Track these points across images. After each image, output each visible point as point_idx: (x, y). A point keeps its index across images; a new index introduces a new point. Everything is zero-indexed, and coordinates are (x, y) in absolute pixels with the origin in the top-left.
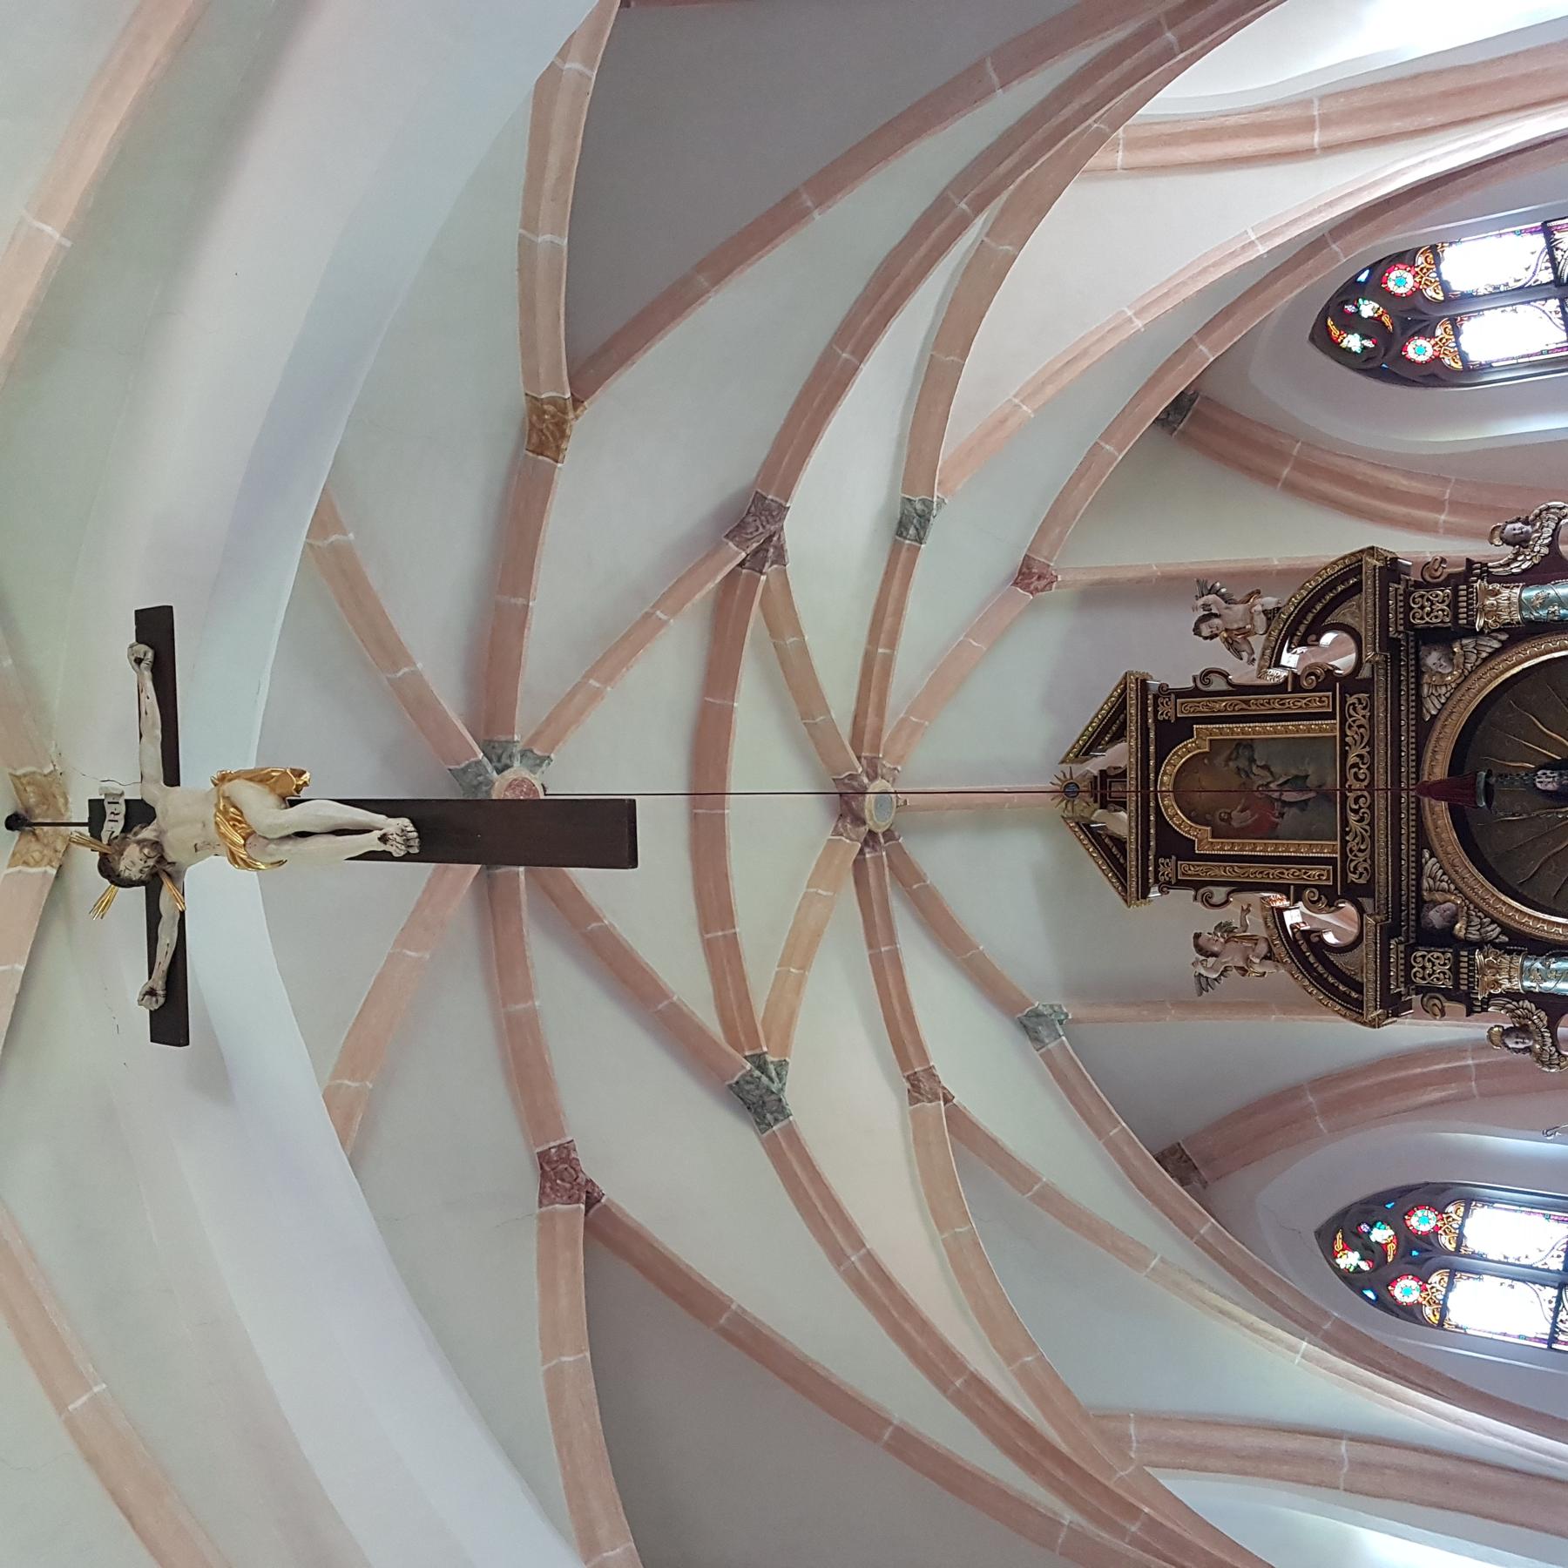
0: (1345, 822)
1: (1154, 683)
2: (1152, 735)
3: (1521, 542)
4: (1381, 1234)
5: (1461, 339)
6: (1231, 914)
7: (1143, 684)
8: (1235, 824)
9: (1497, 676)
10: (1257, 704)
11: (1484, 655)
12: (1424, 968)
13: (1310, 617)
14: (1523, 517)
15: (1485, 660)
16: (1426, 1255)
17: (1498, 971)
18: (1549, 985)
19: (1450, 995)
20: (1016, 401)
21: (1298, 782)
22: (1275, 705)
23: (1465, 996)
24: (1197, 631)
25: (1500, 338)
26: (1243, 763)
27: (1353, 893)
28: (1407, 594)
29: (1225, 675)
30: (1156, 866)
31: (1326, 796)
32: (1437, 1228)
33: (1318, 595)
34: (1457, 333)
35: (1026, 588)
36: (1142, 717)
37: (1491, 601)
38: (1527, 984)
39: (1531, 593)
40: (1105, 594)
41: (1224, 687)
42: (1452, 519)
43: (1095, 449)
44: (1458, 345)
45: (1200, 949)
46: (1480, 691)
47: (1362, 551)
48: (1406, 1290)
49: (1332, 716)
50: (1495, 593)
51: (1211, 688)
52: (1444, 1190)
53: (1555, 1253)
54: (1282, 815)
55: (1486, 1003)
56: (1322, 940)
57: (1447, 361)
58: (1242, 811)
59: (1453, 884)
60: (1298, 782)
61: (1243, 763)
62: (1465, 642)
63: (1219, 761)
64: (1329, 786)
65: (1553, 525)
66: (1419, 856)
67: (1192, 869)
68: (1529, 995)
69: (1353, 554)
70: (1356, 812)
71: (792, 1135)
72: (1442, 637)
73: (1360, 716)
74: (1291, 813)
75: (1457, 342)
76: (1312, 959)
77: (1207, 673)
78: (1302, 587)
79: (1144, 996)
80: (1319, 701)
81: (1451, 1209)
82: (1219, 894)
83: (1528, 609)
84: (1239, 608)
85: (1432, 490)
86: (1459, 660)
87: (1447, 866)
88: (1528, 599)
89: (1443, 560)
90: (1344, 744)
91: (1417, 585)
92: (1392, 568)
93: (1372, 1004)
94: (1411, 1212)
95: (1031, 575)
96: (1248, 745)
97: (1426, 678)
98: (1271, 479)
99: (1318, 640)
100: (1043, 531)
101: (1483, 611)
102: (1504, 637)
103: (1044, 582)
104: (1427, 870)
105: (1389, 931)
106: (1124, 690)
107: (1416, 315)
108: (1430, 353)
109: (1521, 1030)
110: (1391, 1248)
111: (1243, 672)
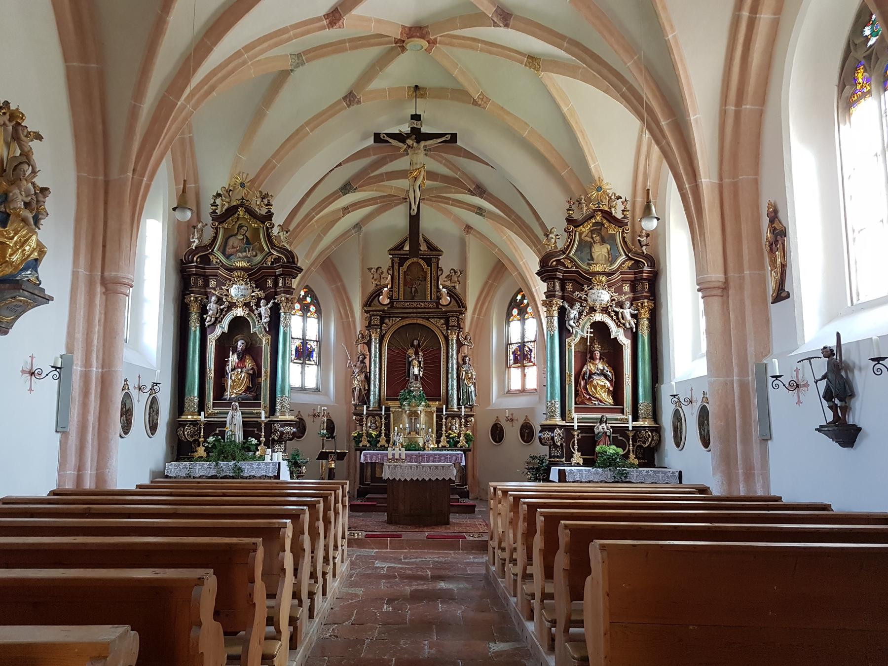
3: (466, 339)
4: (309, 300)
19: (370, 323)
21: (416, 291)
23: (369, 326)
25: (515, 331)
27: (391, 303)
31: (413, 298)
40: (463, 244)
48: (297, 306)
59: (394, 324)
60: (416, 291)
67: (396, 266)
71: (340, 197)
77: (442, 270)
80: (434, 297)
82: (391, 272)
100: (479, 233)
105: (384, 312)
107: (522, 312)
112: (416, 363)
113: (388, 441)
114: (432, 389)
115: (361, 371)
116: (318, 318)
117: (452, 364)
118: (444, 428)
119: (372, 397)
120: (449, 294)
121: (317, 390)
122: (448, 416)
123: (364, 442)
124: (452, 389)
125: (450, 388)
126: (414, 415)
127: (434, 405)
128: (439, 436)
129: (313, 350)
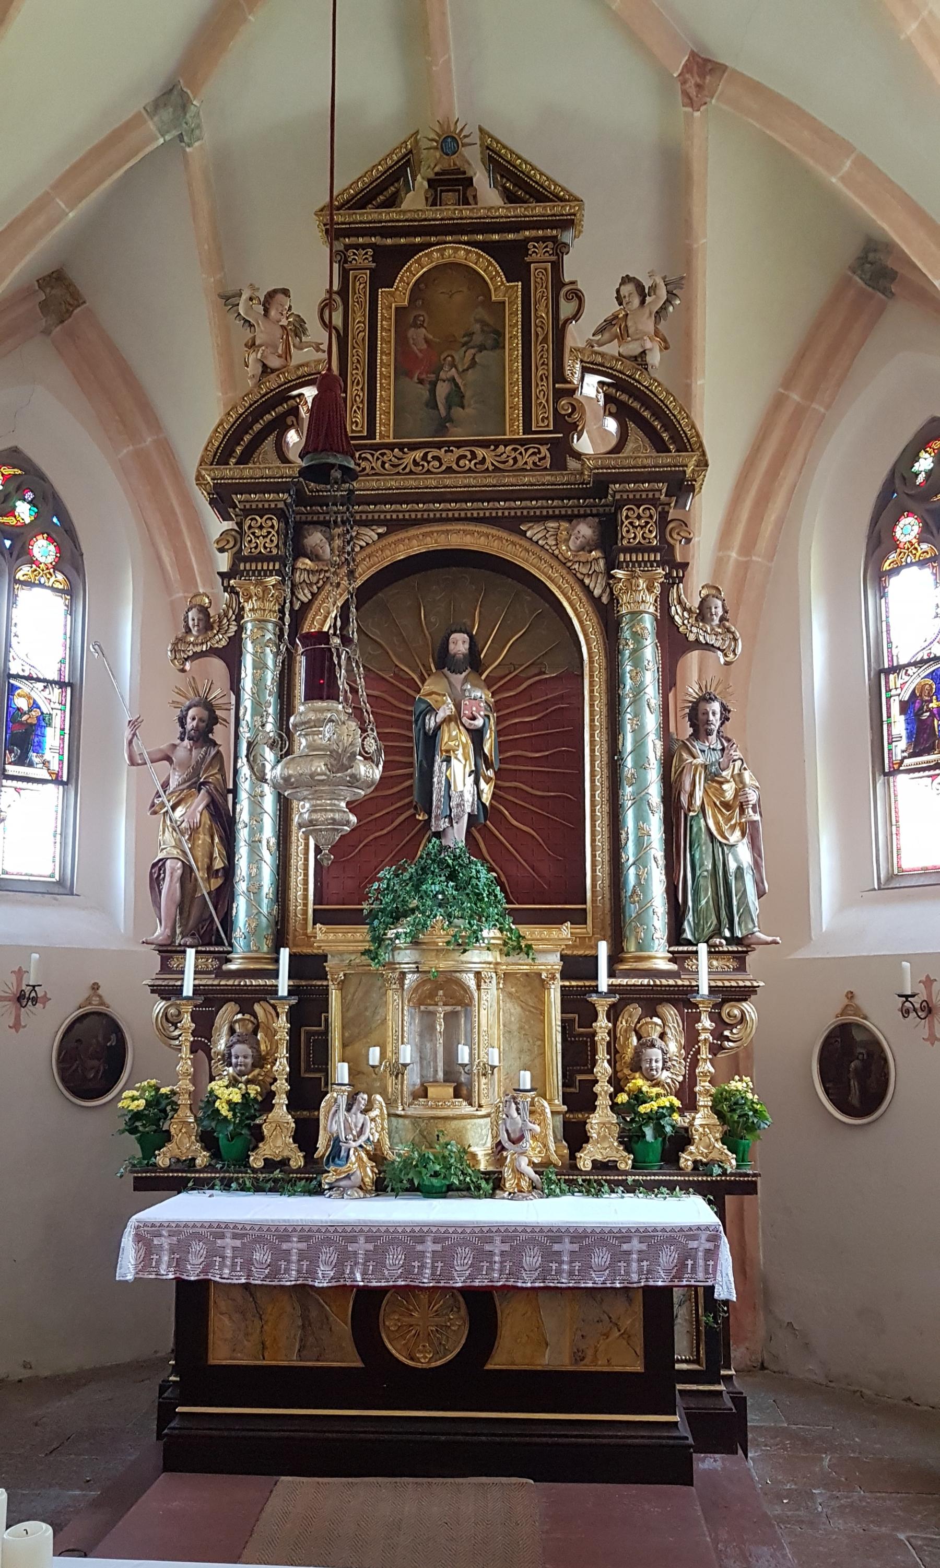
0: (413, 447)
1: (567, 237)
2: (511, 236)
3: (703, 614)
5: (915, 569)
6: (316, 332)
7: (568, 223)
8: (411, 332)
9: (565, 595)
10: (542, 353)
11: (587, 581)
12: (261, 527)
13: (636, 405)
14: (728, 616)
15: (582, 581)
16: (7, 555)
17: (261, 599)
18: (249, 646)
20: (925, 13)
21: (457, 398)
22: (542, 370)
24: (626, 280)
26: (478, 339)
28: (654, 502)
29: (576, 316)
30: (363, 246)
31: (442, 426)
32: (37, 563)
33: (659, 411)
34: (922, 563)
35: (687, 68)
36: (529, 223)
37: (642, 584)
38: (249, 626)
39: (648, 623)
40: (675, 178)
41: (562, 317)
42: (732, 561)
43: (846, 148)
44: (908, 565)
45: (271, 295)
46: (549, 578)
47: (704, 454)
49: (527, 429)
50: (650, 589)
51: (562, 301)
52: (78, 572)
53: (27, 668)
54: (421, 382)
55: (232, 591)
56: (288, 428)
57: (893, 556)
58: (427, 341)
61: (478, 339)
62: (602, 562)
63: (481, 313)
64: (453, 430)
65: (717, 644)
66: (380, 523)
67: (361, 283)
68: (241, 628)
69: (701, 445)
70: (424, 458)
72: (607, 539)
73: (527, 458)
74: (425, 392)
75: (912, 564)
76: (268, 417)
77: (578, 296)
78: (668, 393)
79: (225, 240)
80: (543, 418)
81: (60, 577)
83: (631, 620)
84: (650, 326)
85: (762, 545)
86: (583, 556)
87: (369, 550)
88: (641, 620)
89: (688, 541)
90: (497, 444)
91: (663, 515)
92: (682, 487)
93: (218, 474)
94: (50, 539)
95: (702, 75)
96: (499, 345)
97: (564, 525)
98: (788, 381)
99: (611, 414)
100: (756, 88)
101: (633, 576)
102: (605, 600)
103: (693, 92)
104: (364, 530)
106: (561, 199)
108: (903, 539)
109: (207, 624)
110: (11, 521)
111: (578, 335)
112: (456, 739)
113: (305, 1134)
114: (539, 856)
115: (194, 784)
116: (69, 592)
117: (639, 744)
118: (603, 1068)
119: (241, 907)
120: (620, 411)
121: (60, 888)
122: (624, 998)
123: (184, 1143)
124: (641, 861)
125: (630, 852)
126: (445, 997)
127: (550, 945)
128: (579, 1099)
129: (44, 721)
